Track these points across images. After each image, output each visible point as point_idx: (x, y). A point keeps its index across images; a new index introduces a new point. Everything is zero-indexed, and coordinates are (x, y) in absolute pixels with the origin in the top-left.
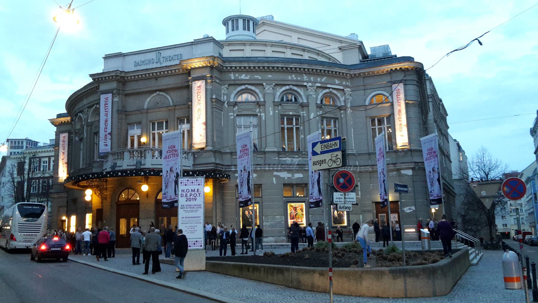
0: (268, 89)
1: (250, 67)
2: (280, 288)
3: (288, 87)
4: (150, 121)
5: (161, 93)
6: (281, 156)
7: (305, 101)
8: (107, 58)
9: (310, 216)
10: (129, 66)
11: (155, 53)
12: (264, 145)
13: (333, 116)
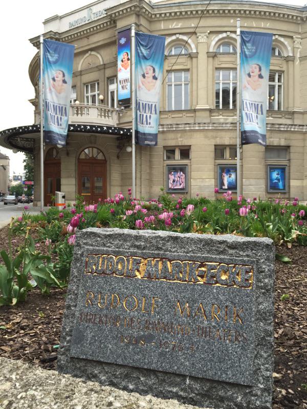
0: (202, 39)
1: (181, 13)
2: (267, 242)
3: (224, 35)
4: (84, 84)
5: (93, 53)
6: (213, 114)
7: (291, 54)
8: (46, 22)
9: (244, 180)
10: (62, 27)
11: (86, 10)
12: (194, 103)
13: (277, 68)
